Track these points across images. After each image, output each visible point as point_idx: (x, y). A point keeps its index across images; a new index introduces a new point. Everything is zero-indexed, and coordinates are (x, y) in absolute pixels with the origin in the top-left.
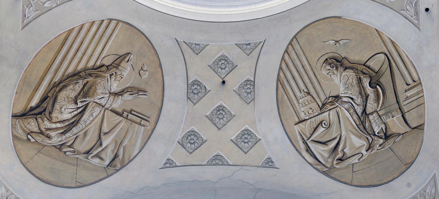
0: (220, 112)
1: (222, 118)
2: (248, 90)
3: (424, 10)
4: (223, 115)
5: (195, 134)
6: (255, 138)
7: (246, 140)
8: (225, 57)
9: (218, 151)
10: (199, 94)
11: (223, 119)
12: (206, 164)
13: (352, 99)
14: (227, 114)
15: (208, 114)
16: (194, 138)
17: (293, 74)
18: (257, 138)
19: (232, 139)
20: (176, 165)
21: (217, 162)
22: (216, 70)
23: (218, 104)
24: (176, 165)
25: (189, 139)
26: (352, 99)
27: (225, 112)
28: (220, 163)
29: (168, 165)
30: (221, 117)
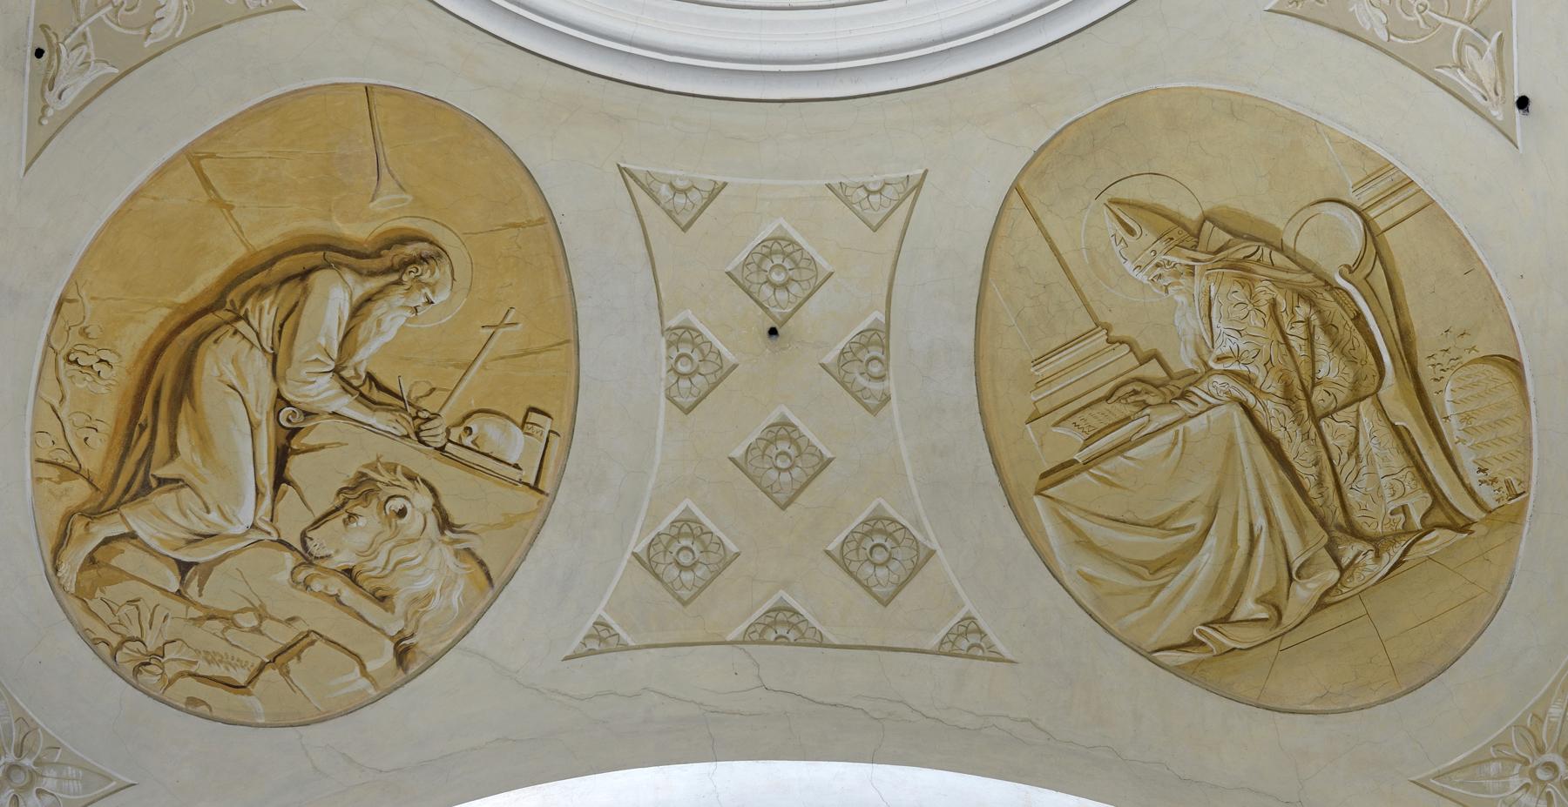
0: (875, 542)
1: (788, 469)
2: (778, 274)
3: (1517, 95)
4: (886, 550)
5: (790, 620)
6: (718, 361)
7: (785, 461)
8: (784, 243)
9: (688, 502)
10: (697, 379)
11: (888, 565)
12: (741, 639)
13: (1248, 380)
14: (804, 456)
15: (738, 453)
16: (776, 632)
17: (746, 57)
18: (723, 358)
19: (830, 548)
20: (621, 642)
21: (782, 631)
22: (754, 291)
23: (773, 418)
24: (621, 642)
25: (674, 553)
26: (1248, 380)
27: (895, 540)
28: (792, 636)
29: (594, 645)
30: (879, 556)
